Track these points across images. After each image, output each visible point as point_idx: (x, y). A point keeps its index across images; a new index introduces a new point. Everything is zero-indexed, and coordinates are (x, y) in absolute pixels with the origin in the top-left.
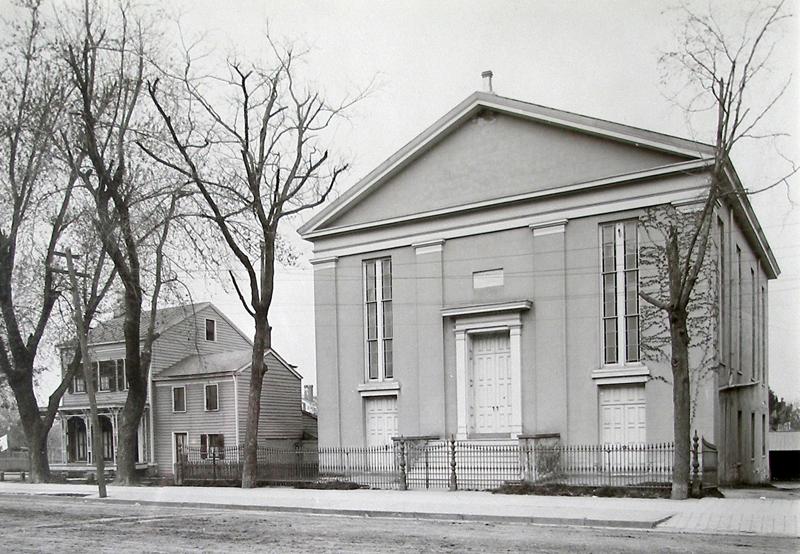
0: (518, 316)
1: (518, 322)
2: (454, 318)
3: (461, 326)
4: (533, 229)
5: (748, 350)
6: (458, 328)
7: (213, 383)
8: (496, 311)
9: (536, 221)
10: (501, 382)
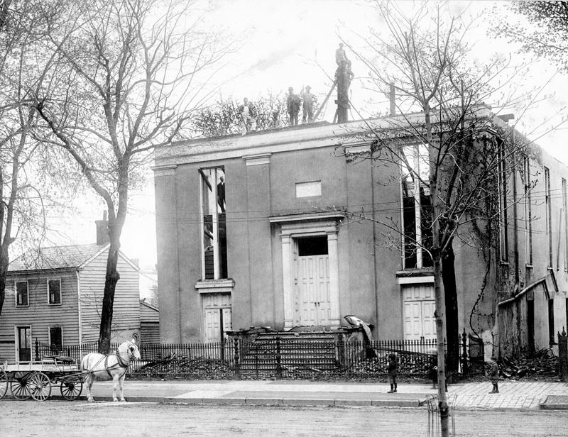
0: (334, 223)
1: (333, 229)
2: (280, 224)
3: (286, 231)
4: (246, 160)
5: (511, 249)
6: (284, 232)
7: (55, 278)
8: (315, 219)
9: (258, 153)
10: (321, 280)
